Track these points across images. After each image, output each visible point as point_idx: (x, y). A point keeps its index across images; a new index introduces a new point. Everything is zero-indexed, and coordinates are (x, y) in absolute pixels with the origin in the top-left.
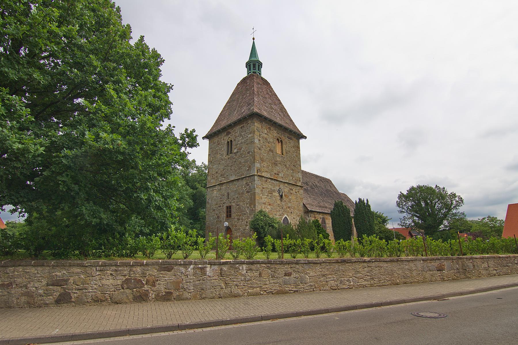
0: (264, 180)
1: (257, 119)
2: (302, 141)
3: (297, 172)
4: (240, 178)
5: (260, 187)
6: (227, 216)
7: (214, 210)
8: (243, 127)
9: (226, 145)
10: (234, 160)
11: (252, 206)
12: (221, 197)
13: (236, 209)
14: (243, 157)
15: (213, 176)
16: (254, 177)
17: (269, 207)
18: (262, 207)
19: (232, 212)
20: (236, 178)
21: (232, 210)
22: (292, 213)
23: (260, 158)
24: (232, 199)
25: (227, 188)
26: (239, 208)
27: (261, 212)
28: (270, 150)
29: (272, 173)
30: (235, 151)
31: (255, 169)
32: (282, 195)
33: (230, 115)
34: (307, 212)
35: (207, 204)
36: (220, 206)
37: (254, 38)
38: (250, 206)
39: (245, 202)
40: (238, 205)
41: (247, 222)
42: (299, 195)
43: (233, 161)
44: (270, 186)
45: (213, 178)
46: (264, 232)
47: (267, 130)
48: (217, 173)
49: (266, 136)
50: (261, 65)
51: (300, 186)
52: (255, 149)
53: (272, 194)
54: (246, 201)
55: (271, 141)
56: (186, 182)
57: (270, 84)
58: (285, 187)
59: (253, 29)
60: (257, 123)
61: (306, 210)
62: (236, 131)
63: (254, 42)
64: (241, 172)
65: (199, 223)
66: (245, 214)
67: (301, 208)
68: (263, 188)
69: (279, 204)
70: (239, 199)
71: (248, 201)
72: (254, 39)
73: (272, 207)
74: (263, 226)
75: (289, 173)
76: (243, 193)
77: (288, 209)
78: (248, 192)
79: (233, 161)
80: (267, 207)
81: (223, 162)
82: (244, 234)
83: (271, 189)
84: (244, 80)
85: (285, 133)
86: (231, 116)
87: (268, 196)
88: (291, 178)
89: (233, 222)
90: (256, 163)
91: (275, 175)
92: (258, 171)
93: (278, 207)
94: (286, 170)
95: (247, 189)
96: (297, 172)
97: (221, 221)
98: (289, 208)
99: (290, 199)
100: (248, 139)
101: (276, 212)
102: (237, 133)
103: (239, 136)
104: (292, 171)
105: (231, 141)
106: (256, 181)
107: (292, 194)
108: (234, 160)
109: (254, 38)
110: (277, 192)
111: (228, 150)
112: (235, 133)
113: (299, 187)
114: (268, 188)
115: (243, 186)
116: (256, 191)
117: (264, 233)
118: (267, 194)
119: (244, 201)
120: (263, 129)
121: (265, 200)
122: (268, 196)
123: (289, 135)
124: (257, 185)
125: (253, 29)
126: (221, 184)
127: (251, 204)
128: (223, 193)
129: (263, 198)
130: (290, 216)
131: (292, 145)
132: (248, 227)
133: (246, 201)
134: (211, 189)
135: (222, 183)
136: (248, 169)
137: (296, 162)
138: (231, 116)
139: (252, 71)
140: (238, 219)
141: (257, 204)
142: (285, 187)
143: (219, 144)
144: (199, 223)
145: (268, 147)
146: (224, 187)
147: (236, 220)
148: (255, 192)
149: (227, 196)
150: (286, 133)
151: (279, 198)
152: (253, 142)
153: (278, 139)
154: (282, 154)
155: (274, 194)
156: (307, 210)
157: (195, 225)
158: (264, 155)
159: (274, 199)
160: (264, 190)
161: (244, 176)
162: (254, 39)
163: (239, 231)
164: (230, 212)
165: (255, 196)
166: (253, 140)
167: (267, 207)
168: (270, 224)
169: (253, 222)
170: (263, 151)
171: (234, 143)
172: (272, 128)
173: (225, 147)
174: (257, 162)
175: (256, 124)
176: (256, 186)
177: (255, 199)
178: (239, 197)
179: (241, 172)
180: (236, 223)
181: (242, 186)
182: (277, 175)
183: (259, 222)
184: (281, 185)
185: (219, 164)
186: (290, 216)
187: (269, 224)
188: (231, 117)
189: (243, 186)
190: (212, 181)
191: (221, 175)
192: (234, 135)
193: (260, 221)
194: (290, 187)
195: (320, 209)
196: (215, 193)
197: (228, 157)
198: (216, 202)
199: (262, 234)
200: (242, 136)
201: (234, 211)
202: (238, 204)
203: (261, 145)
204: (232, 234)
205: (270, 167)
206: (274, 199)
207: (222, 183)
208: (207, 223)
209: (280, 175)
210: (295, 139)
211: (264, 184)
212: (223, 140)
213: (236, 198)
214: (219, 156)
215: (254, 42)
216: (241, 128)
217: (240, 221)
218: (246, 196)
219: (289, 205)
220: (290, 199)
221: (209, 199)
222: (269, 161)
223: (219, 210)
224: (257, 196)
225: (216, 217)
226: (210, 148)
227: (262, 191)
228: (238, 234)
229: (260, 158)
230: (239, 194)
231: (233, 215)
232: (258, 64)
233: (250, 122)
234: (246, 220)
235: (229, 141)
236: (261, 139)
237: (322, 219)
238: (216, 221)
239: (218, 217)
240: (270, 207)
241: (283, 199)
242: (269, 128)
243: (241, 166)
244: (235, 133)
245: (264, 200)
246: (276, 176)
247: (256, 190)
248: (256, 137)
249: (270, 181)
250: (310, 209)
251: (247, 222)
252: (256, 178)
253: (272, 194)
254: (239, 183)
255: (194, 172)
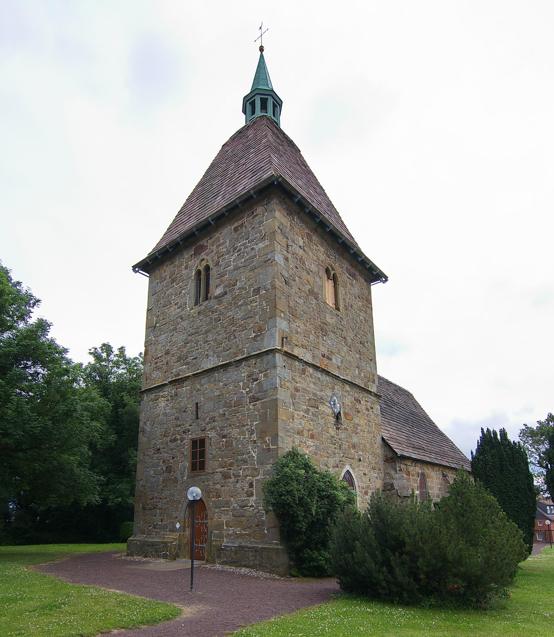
0: (299, 369)
1: (280, 202)
2: (376, 288)
3: (368, 358)
4: (230, 363)
5: (288, 384)
6: (194, 467)
7: (159, 450)
8: (242, 226)
9: (193, 280)
10: (215, 316)
11: (267, 438)
12: (176, 415)
13: (220, 448)
14: (242, 305)
15: (156, 363)
16: (275, 357)
17: (310, 442)
18: (293, 442)
19: (208, 456)
20: (220, 364)
21: (207, 450)
22: (360, 460)
23: (289, 306)
24: (207, 420)
25: (194, 392)
26: (229, 444)
27: (293, 455)
28: (311, 292)
29: (317, 352)
30: (218, 291)
31: (277, 334)
32: (339, 413)
33: (206, 206)
34: (392, 458)
35: (140, 435)
36: (175, 440)
37: (262, 46)
38: (261, 437)
39: (245, 428)
40: (224, 437)
41: (251, 485)
42: (373, 416)
43: (211, 319)
44: (312, 385)
45: (157, 368)
46: (305, 517)
47: (303, 238)
48: (167, 353)
49: (301, 252)
50: (278, 107)
51: (376, 395)
52: (276, 280)
53: (317, 408)
54: (247, 425)
55: (314, 268)
56: (100, 391)
57: (300, 151)
58: (345, 394)
59: (261, 28)
60: (280, 211)
61: (388, 454)
62: (222, 241)
63: (262, 57)
64: (234, 346)
65: (211, 451)
66: (245, 462)
67: (378, 449)
68: (297, 390)
69: (333, 437)
70: (229, 419)
71: (255, 423)
72: (261, 49)
73: (317, 443)
74: (302, 498)
75: (352, 359)
76: (239, 403)
77: (353, 451)
78: (254, 399)
79: (211, 319)
80: (305, 442)
81: (185, 324)
82: (243, 519)
83: (315, 395)
84: (240, 133)
85: (341, 259)
86: (208, 208)
87: (307, 411)
88: (357, 372)
89: (211, 483)
90: (278, 319)
91: (322, 360)
92: (283, 341)
93: (331, 445)
94: (345, 349)
95: (250, 391)
96: (368, 358)
97: (176, 481)
98: (354, 447)
99: (356, 426)
100: (255, 256)
101: (328, 457)
102: (223, 244)
103: (229, 252)
104: (357, 356)
105: (207, 268)
106: (279, 368)
107: (359, 412)
108: (215, 316)
109: (262, 46)
110: (329, 405)
111: (197, 293)
112: (217, 247)
113: (372, 397)
114: (308, 392)
115: (241, 384)
116: (279, 396)
117: (307, 518)
118: (305, 407)
119: (244, 426)
120: (294, 234)
121: (300, 424)
122: (307, 411)
123: (350, 266)
124: (280, 379)
125: (261, 28)
126: (178, 382)
127: (262, 434)
128: (182, 404)
129: (296, 416)
130: (357, 469)
131: (357, 291)
132: (254, 498)
133: (247, 425)
134: (153, 396)
135: (180, 377)
136: (255, 336)
137: (366, 336)
138: (208, 208)
139: (259, 113)
140: (226, 476)
141: (281, 434)
142: (345, 394)
143: (173, 281)
144: (129, 480)
145: (307, 283)
146: (185, 389)
147: (218, 477)
148: (277, 399)
149: (195, 413)
150: (344, 259)
151: (333, 420)
152: (268, 262)
153: (327, 271)
154: (338, 309)
155: (322, 408)
156: (390, 455)
157: (118, 485)
158: (296, 301)
159: (322, 421)
160: (298, 394)
161: (244, 356)
162: (261, 49)
163: (228, 510)
164: (203, 454)
165: (277, 410)
166: (269, 257)
167: (305, 442)
168: (323, 491)
169: (274, 486)
170: (295, 289)
171: (214, 273)
172: (315, 238)
173: (191, 286)
174: (280, 317)
175: (277, 214)
176: (278, 381)
177: (277, 418)
178: (227, 413)
179: (234, 346)
180: (218, 486)
181: (236, 384)
182: (328, 361)
183: (292, 486)
184: (336, 388)
185: (175, 329)
186: (357, 469)
187: (319, 491)
188: (206, 211)
189: (241, 384)
190: (155, 376)
191: (179, 359)
192: (215, 252)
193: (295, 484)
194: (356, 395)
195: (415, 452)
196: (163, 404)
197: (197, 309)
198: (164, 430)
199: (299, 521)
200: (238, 252)
201: (214, 452)
202: (225, 432)
203: (290, 272)
204: (207, 515)
205: (311, 336)
206: (322, 421)
207: (181, 378)
208: (139, 485)
209: (334, 360)
210: (362, 280)
211: (298, 379)
212: (186, 268)
213: (220, 417)
214: (174, 311)
215: (262, 57)
216: (236, 230)
217: (230, 480)
218: (249, 409)
219: (355, 440)
220: (356, 426)
221: (145, 422)
222: (310, 319)
223: (172, 449)
224: (280, 411)
225: (162, 469)
226: (152, 293)
227: (293, 396)
228: (224, 519)
229: (289, 306)
230: (228, 405)
231: (211, 464)
232: (272, 100)
233: (260, 210)
234: (248, 478)
235: (200, 268)
236: (290, 256)
237: (420, 477)
238: (164, 480)
239: (169, 469)
240: (312, 444)
241: (341, 424)
242: (309, 236)
243: (234, 331)
244: (217, 247)
245: (299, 423)
246: (326, 361)
247: (279, 392)
248: (278, 247)
249: (311, 372)
250: (399, 453)
251: (251, 485)
252: (279, 359)
253: (317, 408)
254: (228, 375)
255: (120, 371)
